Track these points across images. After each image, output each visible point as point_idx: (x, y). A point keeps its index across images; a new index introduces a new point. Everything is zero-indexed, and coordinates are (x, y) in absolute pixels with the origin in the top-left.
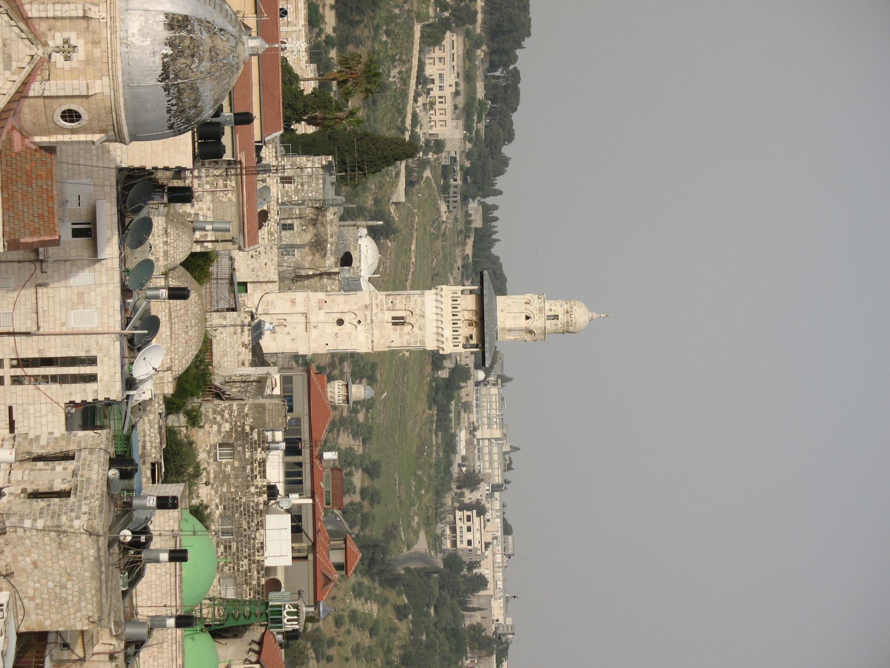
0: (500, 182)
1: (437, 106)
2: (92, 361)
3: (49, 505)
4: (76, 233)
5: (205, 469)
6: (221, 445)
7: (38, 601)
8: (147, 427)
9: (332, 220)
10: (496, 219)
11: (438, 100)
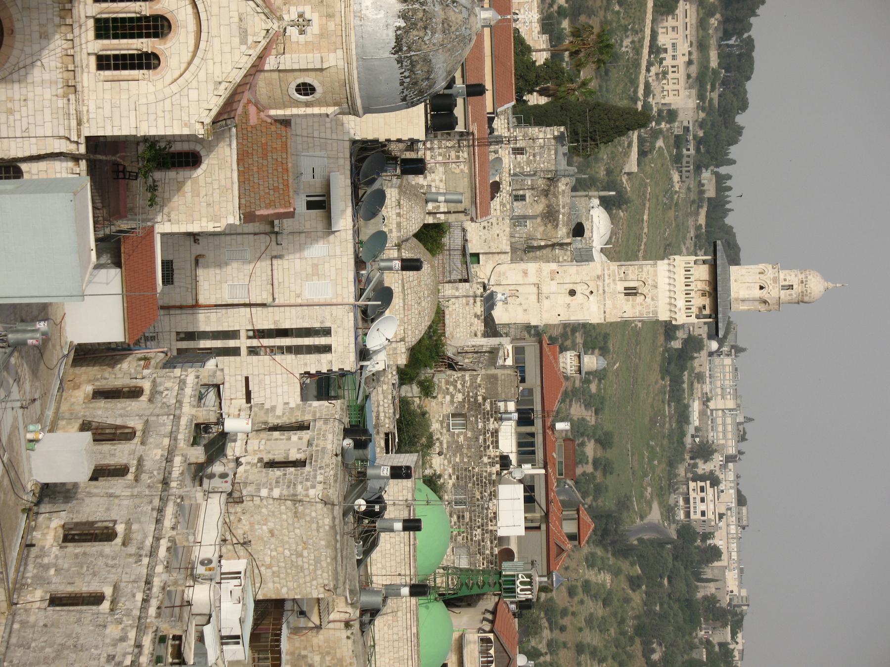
0: (734, 152)
1: (670, 75)
2: (327, 332)
3: (285, 474)
4: (311, 205)
5: (438, 439)
6: (454, 415)
7: (275, 569)
8: (381, 397)
9: (564, 191)
10: (730, 189)
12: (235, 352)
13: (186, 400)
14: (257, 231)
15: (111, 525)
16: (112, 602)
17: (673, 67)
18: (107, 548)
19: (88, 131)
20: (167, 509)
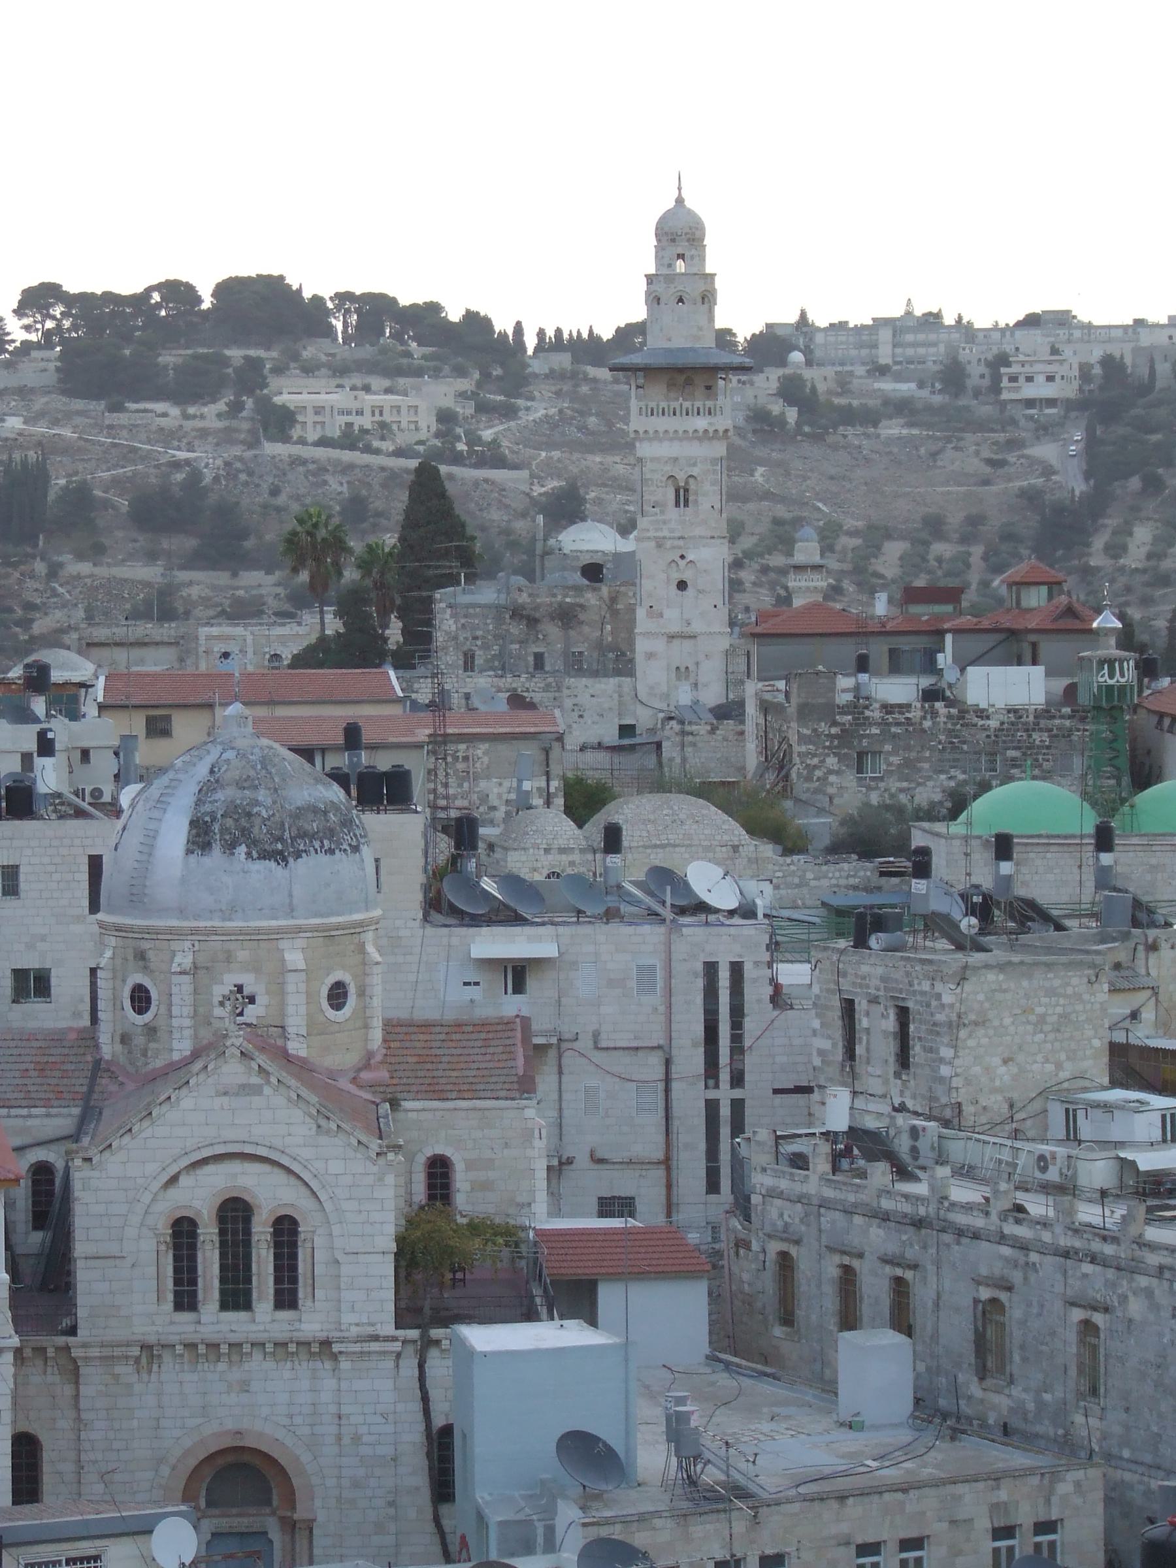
0: (503, 324)
1: (387, 418)
2: (711, 969)
3: (920, 1038)
4: (519, 988)
5: (892, 796)
6: (860, 771)
7: (1063, 1056)
8: (825, 883)
9: (530, 595)
10: (559, 332)
11: (377, 418)
12: (738, 1106)
13: (798, 1188)
14: (555, 1069)
15: (980, 1307)
16: (1095, 1309)
17: (373, 415)
18: (1015, 1311)
19: (388, 1328)
20: (958, 1221)
